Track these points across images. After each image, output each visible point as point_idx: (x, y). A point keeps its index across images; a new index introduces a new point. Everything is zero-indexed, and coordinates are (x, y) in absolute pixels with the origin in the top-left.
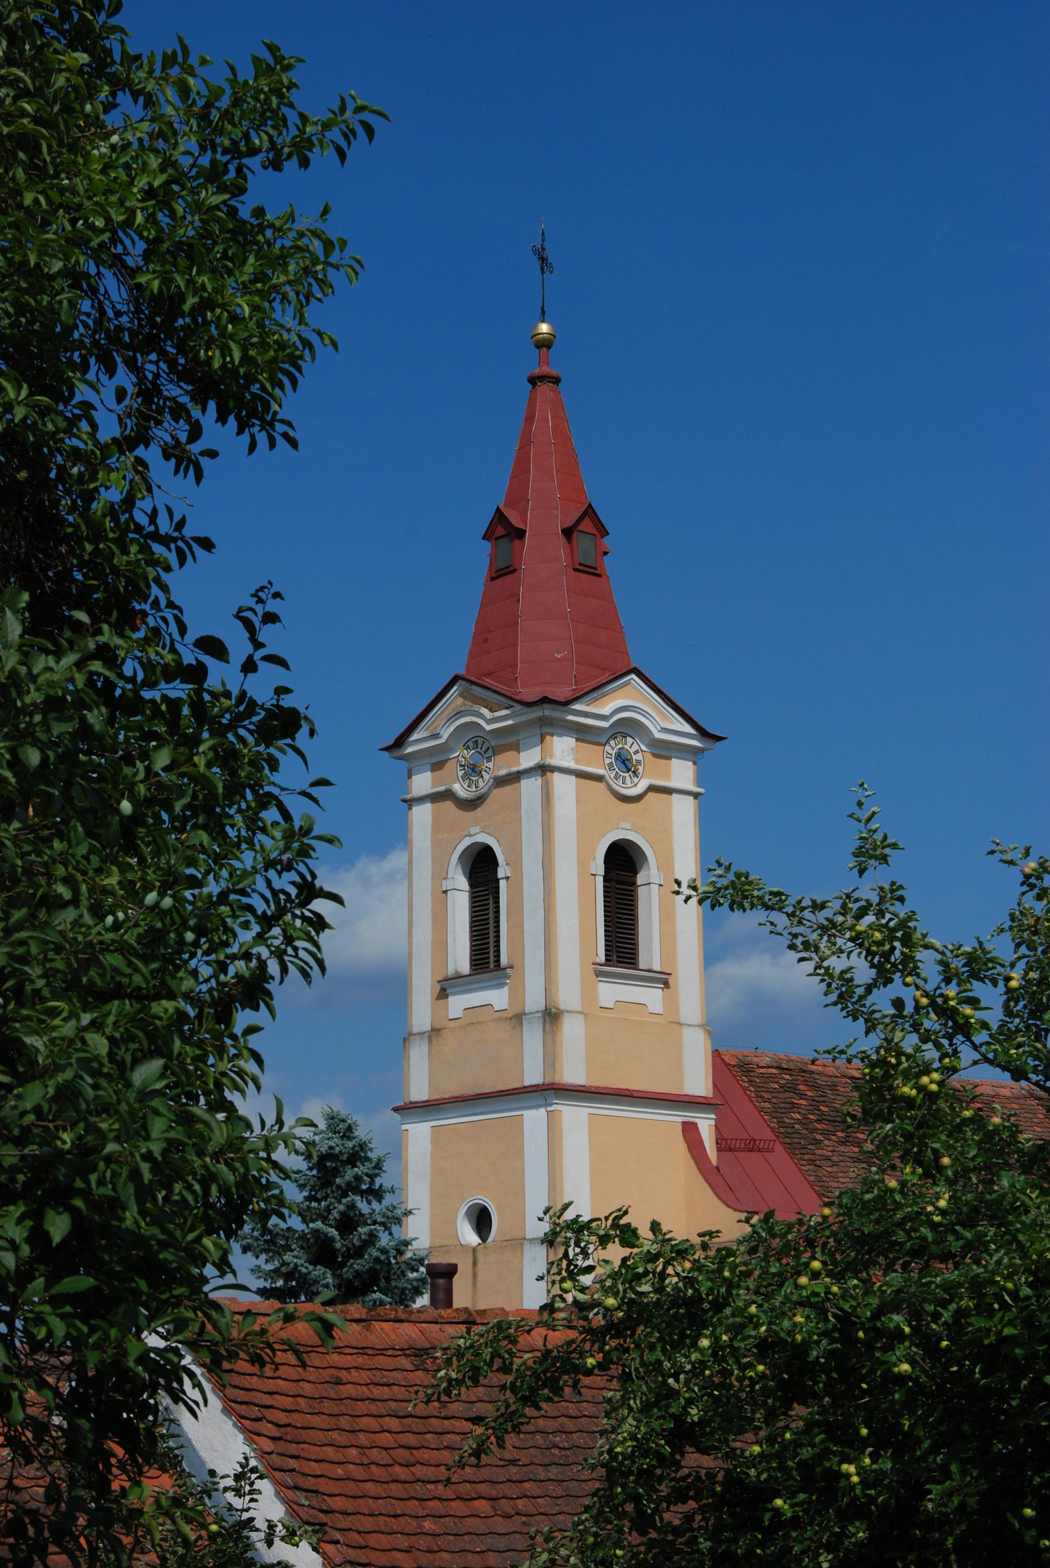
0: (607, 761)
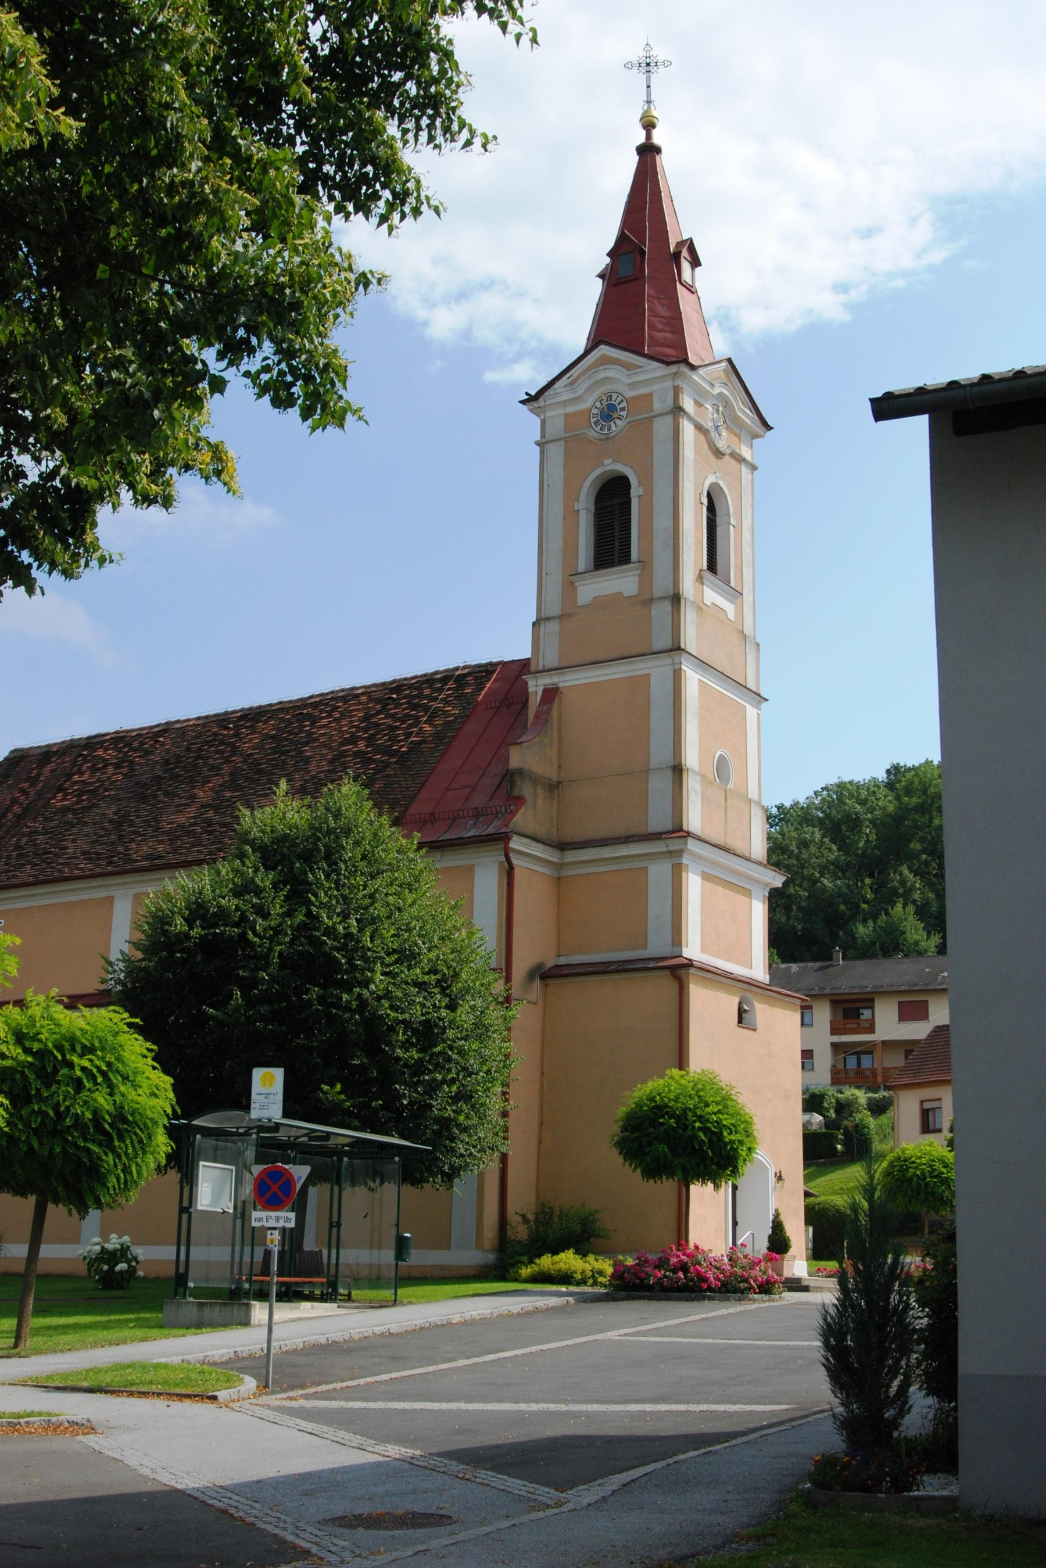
0: (593, 420)
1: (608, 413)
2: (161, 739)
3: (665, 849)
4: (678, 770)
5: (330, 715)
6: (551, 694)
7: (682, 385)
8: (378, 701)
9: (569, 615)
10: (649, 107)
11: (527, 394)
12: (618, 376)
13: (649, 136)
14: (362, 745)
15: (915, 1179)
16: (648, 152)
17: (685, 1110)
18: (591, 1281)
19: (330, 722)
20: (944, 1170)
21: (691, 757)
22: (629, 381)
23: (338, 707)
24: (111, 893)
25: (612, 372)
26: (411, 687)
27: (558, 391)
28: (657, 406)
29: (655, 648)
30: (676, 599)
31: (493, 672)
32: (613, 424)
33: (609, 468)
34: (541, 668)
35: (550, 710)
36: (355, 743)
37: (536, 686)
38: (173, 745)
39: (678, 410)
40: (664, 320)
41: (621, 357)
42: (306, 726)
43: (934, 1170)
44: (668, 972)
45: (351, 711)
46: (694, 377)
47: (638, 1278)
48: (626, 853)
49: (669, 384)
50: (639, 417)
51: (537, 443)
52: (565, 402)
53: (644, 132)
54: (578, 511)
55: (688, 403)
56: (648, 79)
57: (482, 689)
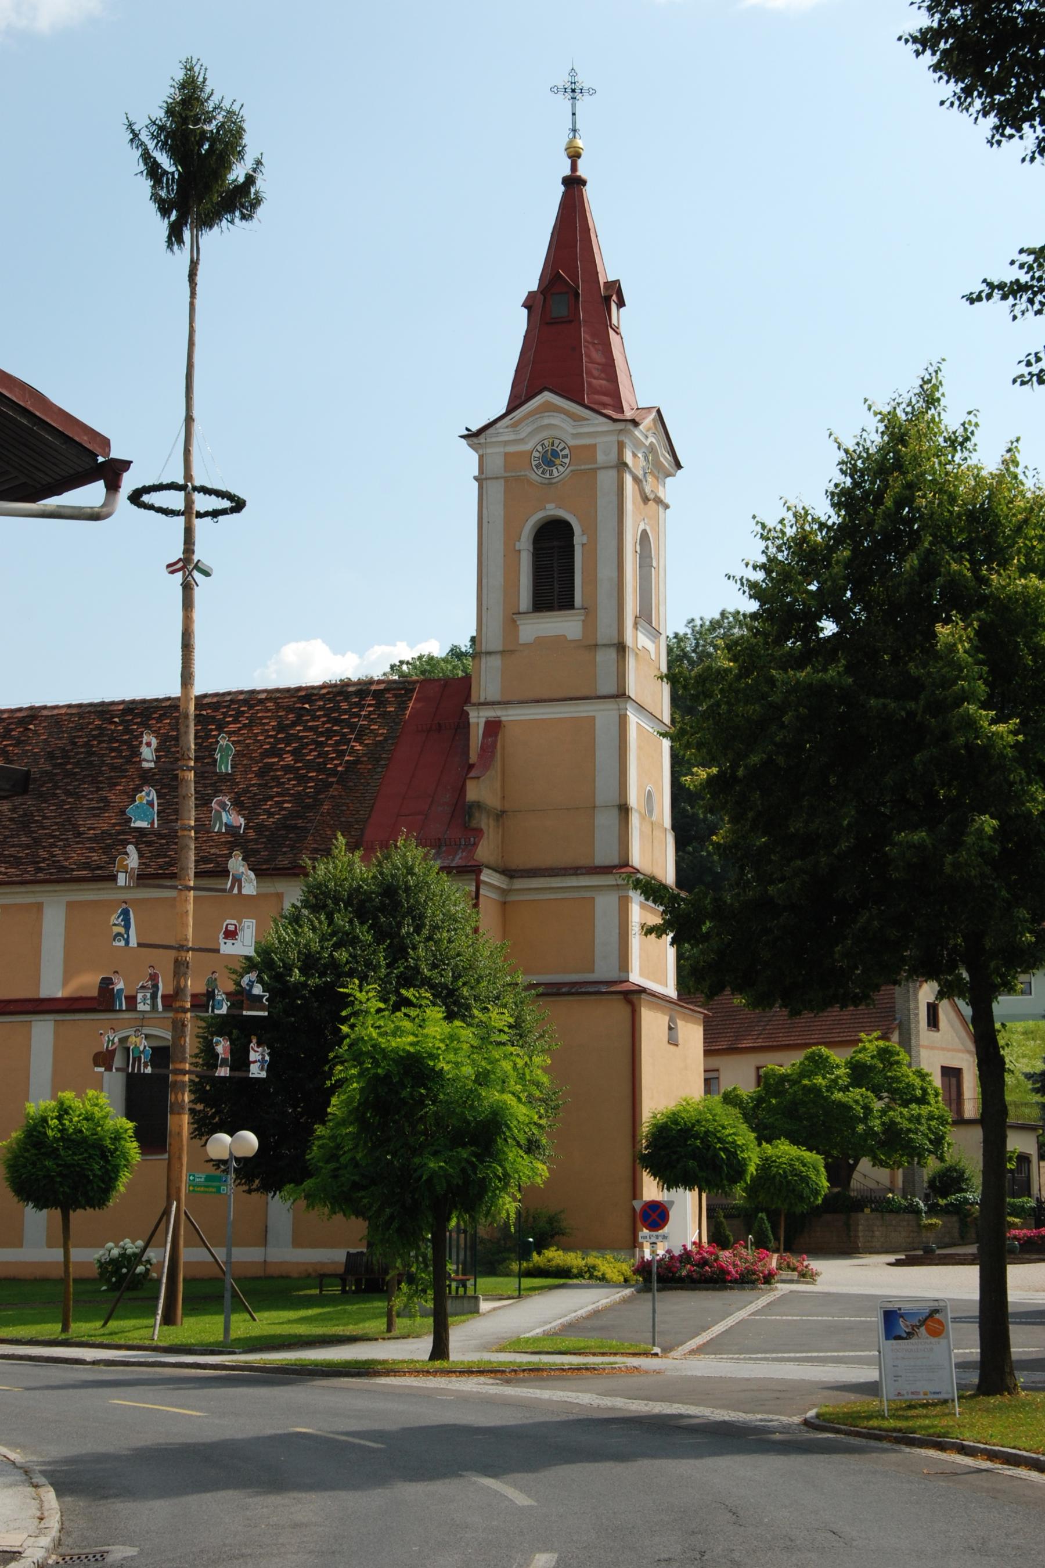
0: (534, 463)
1: (550, 458)
2: (32, 727)
3: (614, 883)
4: (624, 809)
5: (236, 721)
6: (493, 727)
7: (626, 441)
8: (290, 710)
9: (512, 652)
10: (574, 136)
11: (467, 429)
12: (562, 425)
13: (574, 167)
14: (289, 759)
15: (778, 1177)
16: (573, 184)
17: (707, 1132)
18: (587, 1275)
19: (240, 729)
20: (803, 1169)
21: (634, 799)
22: (574, 432)
23: (243, 712)
24: (40, 900)
25: (556, 420)
26: (322, 697)
27: (501, 431)
28: (601, 458)
29: (600, 693)
30: (621, 648)
31: (413, 690)
32: (555, 470)
33: (552, 513)
34: (482, 700)
35: (495, 743)
36: (280, 756)
37: (478, 718)
38: (50, 734)
39: (622, 465)
40: (600, 367)
41: (566, 407)
42: (212, 730)
43: (795, 1169)
44: (621, 997)
45: (261, 718)
46: (636, 433)
47: (670, 1272)
48: (575, 884)
49: (613, 438)
50: (583, 467)
51: (475, 478)
52: (506, 442)
53: (569, 161)
54: (519, 551)
55: (629, 458)
56: (574, 106)
57: (406, 708)
